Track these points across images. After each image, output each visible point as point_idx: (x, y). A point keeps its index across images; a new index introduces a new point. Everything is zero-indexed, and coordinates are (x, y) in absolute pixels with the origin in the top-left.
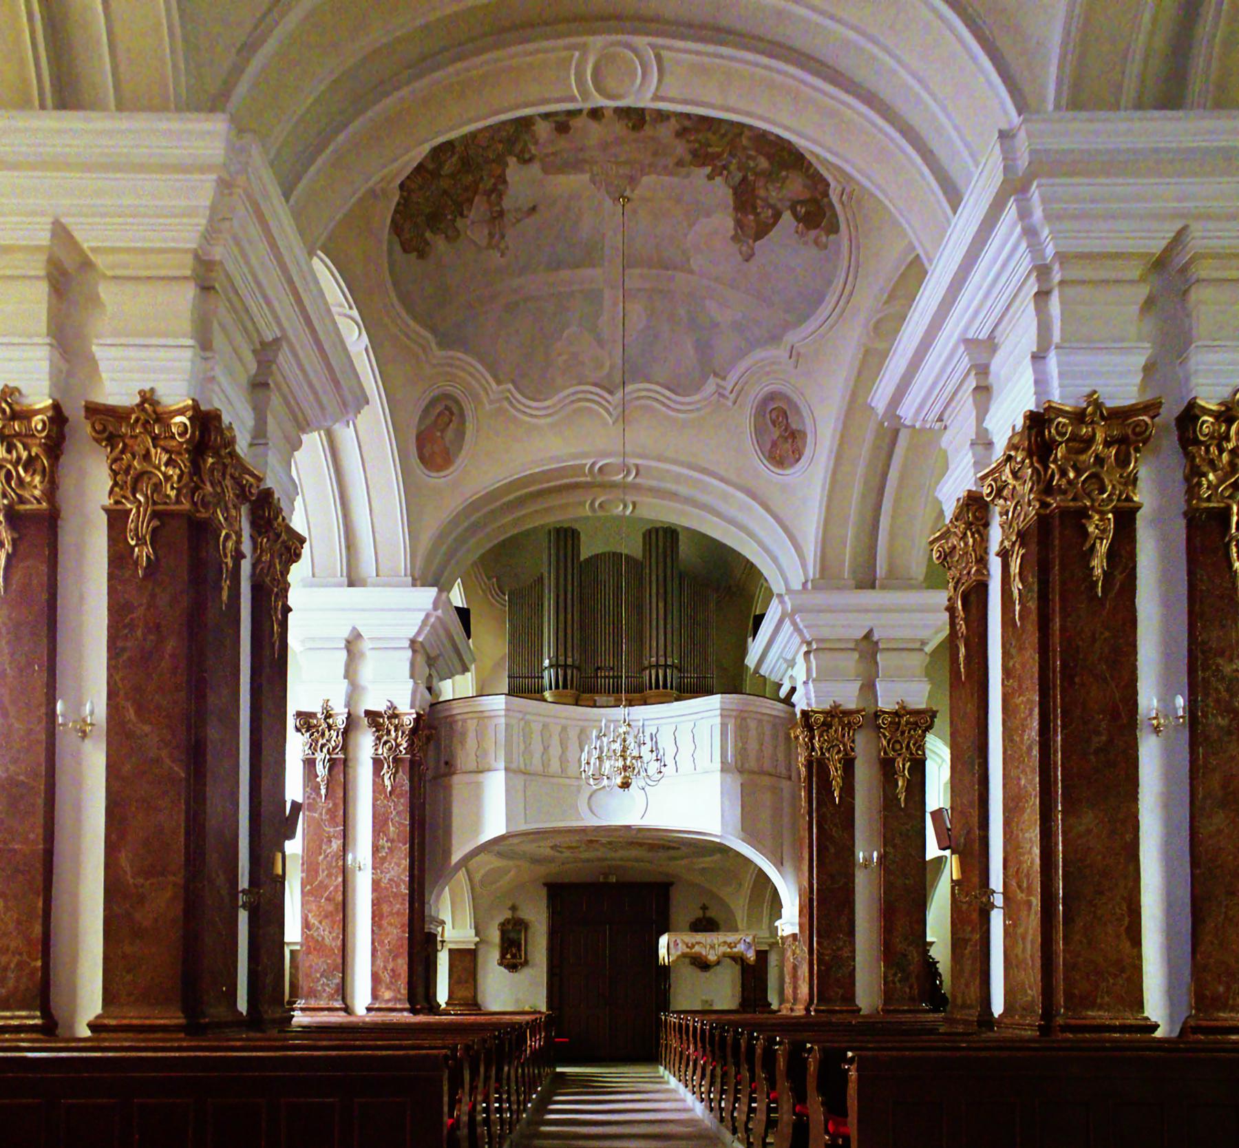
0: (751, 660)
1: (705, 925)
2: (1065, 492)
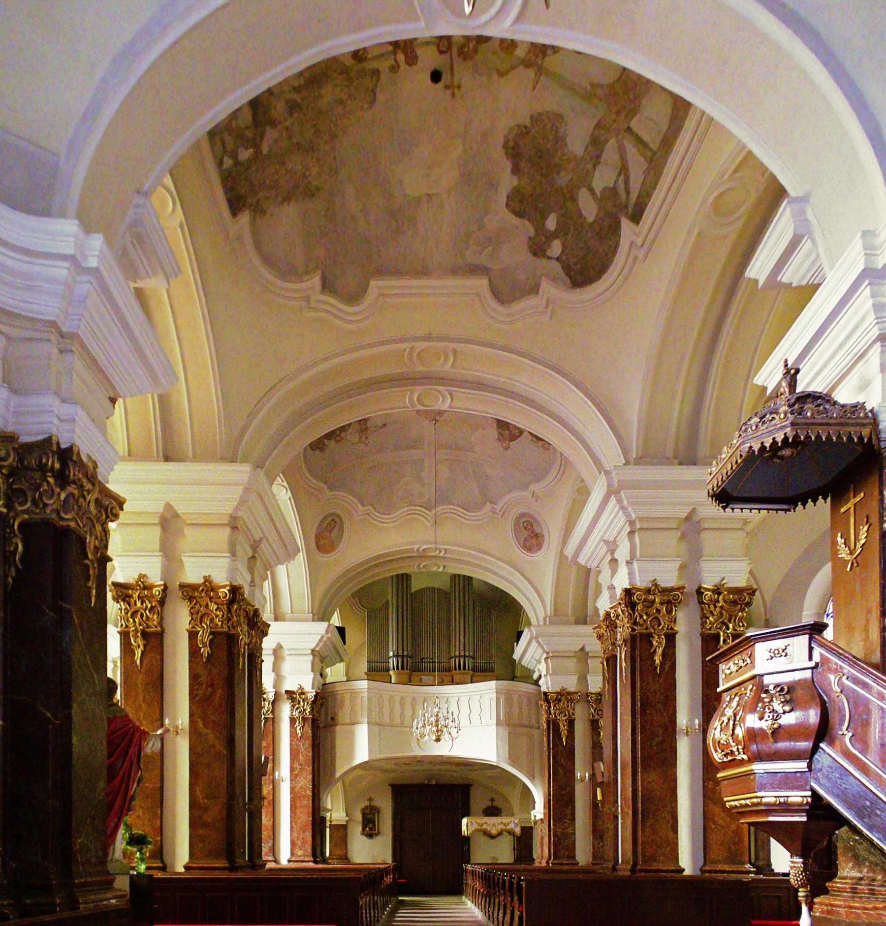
0: (516, 656)
1: (492, 811)
2: (642, 625)
